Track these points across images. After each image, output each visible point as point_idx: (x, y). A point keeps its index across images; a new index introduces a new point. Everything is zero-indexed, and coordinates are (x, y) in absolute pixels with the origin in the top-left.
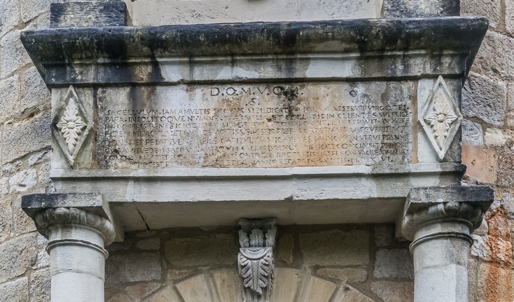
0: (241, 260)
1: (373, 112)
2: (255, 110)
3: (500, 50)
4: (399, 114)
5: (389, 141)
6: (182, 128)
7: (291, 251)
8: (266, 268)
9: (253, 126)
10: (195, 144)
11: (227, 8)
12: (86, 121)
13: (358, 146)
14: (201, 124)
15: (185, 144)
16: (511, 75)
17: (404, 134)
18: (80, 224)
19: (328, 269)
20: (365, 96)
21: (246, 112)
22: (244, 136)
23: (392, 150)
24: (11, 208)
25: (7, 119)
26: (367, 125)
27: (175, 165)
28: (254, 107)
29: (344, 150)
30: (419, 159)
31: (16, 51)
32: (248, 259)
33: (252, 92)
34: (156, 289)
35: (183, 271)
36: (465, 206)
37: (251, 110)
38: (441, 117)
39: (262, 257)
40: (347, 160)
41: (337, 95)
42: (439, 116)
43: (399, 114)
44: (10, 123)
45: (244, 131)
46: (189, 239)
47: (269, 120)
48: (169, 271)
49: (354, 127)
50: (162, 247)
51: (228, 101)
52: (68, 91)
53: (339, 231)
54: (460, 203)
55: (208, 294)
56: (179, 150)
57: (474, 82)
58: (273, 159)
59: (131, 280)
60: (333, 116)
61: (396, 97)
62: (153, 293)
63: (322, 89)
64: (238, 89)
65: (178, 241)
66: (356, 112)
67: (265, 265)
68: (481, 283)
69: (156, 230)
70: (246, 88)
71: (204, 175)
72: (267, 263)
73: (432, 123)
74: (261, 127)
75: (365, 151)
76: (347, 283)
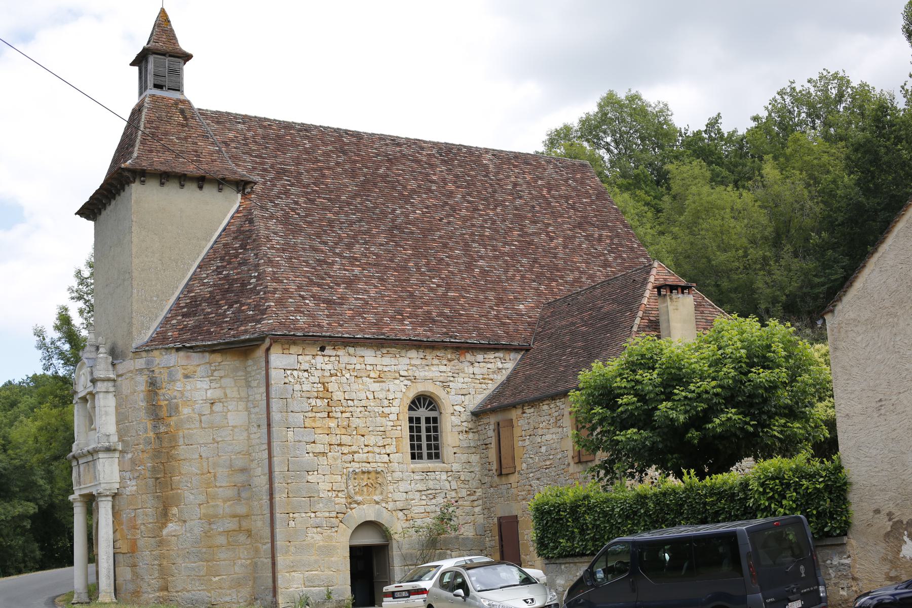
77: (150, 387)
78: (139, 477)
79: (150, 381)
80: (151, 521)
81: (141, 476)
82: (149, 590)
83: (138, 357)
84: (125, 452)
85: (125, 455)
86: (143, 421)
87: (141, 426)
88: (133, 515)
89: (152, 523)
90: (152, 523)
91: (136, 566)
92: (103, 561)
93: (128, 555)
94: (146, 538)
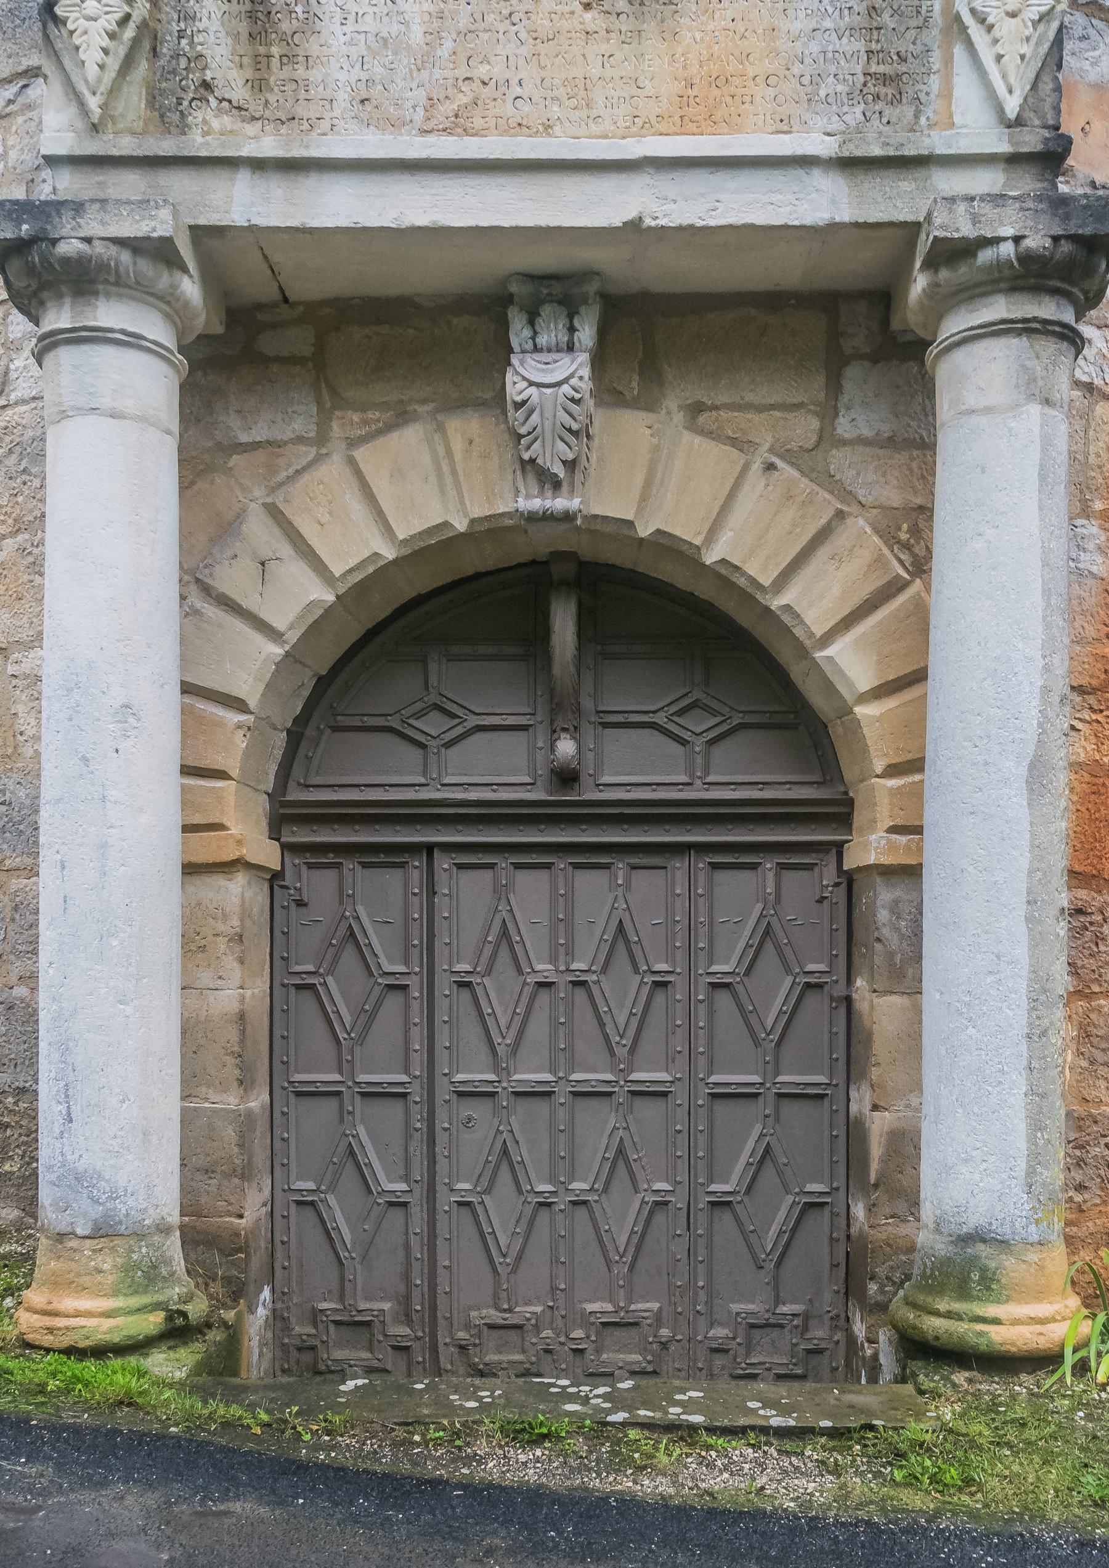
0: (515, 388)
5: (881, 69)
6: (369, 24)
8: (574, 408)
9: (547, 23)
13: (806, 80)
15: (378, 70)
22: (523, 51)
23: (889, 91)
26: (828, 24)
27: (352, 125)
29: (771, 92)
30: (957, 119)
32: (531, 384)
36: (1066, 247)
39: (565, 381)
45: (523, 35)
46: (385, 329)
49: (796, 27)
53: (753, 312)
55: (432, 478)
59: (244, 438)
62: (298, 472)
67: (573, 400)
68: (1098, 455)
72: (577, 396)
73: (990, 20)
74: (566, 25)
75: (823, 94)
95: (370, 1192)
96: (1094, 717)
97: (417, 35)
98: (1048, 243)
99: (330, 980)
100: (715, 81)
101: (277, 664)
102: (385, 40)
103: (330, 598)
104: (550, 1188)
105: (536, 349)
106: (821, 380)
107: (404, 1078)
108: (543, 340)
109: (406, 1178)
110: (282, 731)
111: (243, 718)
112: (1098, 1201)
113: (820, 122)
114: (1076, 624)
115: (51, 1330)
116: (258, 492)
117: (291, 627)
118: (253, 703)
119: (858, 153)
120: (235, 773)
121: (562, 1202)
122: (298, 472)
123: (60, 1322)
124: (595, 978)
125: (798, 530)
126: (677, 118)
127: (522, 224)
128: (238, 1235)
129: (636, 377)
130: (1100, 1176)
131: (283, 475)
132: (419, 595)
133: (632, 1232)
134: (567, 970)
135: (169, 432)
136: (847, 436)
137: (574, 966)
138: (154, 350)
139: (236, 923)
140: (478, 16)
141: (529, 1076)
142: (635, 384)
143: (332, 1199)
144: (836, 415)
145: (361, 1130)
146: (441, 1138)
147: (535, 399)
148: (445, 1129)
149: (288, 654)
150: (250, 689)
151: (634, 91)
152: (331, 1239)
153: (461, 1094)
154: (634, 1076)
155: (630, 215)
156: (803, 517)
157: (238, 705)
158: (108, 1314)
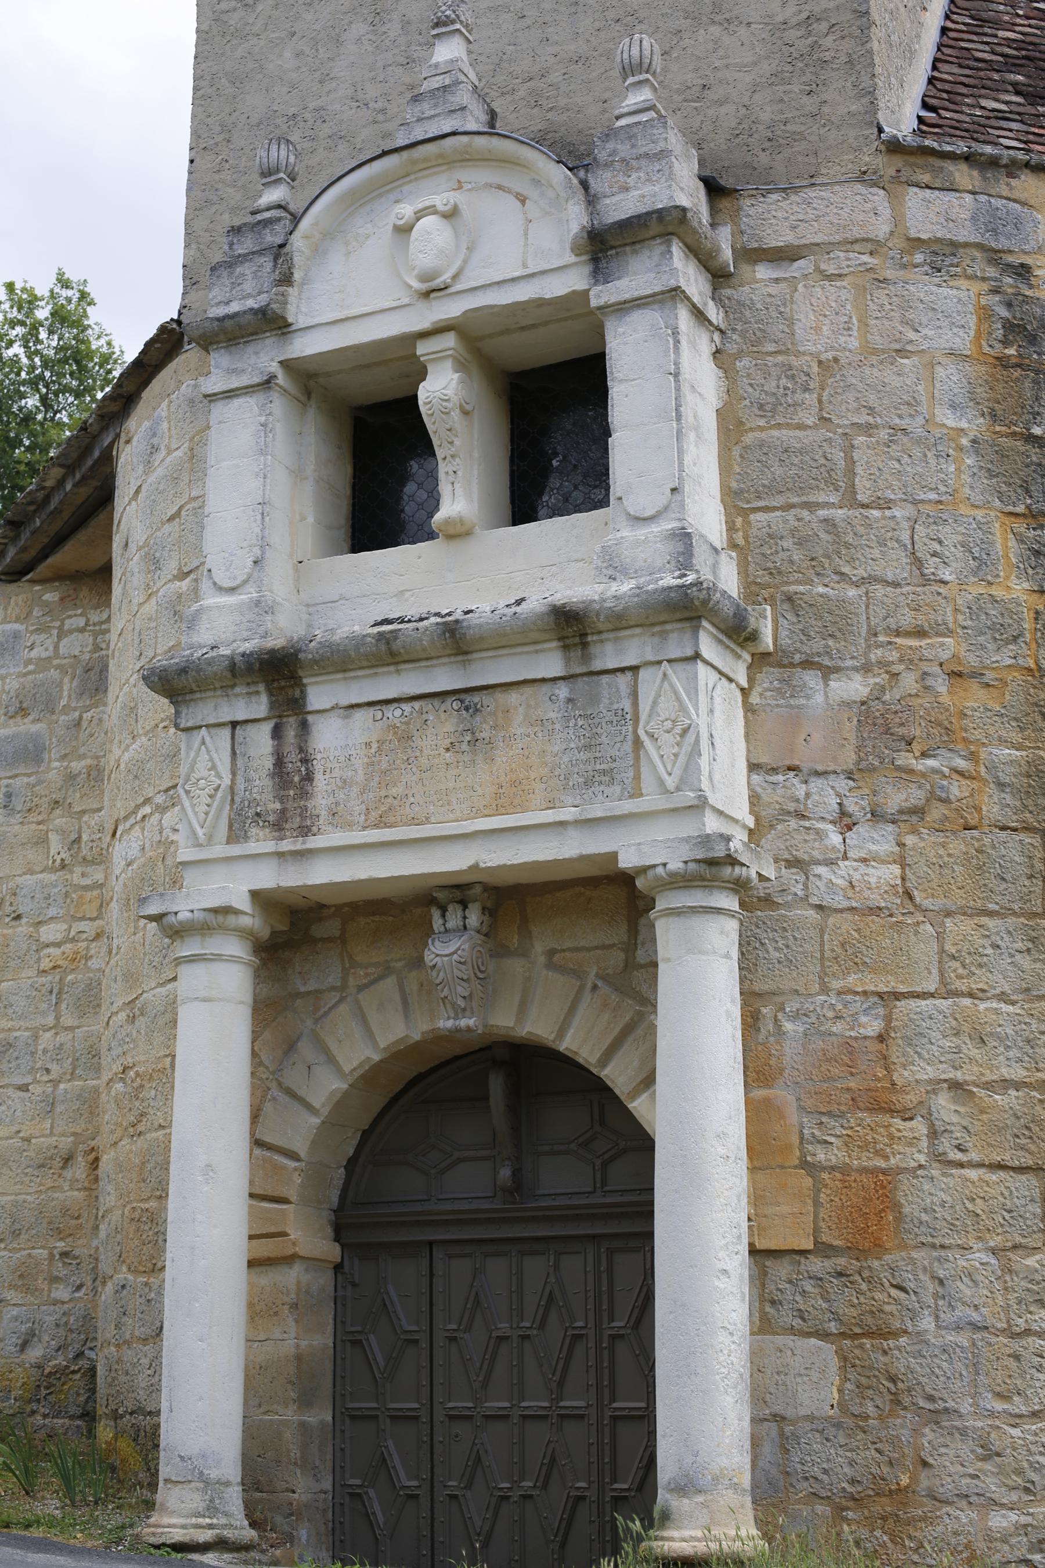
0: (429, 958)
1: (580, 723)
2: (429, 736)
3: (850, 538)
4: (615, 723)
5: (602, 767)
6: (337, 773)
7: (516, 928)
8: (463, 967)
9: (426, 761)
10: (353, 795)
11: (420, 557)
12: (220, 778)
13: (562, 778)
14: (359, 763)
15: (342, 796)
16: (873, 573)
17: (623, 753)
18: (209, 929)
19: (568, 954)
20: (569, 700)
21: (418, 742)
22: (414, 778)
23: (607, 779)
24: (162, 866)
25: (162, 720)
26: (572, 745)
27: (330, 828)
28: (428, 732)
29: (543, 786)
30: (644, 791)
31: (175, 615)
32: (437, 955)
33: (425, 710)
34: (334, 1001)
35: (369, 971)
36: (692, 866)
37: (424, 737)
38: (668, 724)
39: (455, 952)
40: (547, 800)
41: (533, 703)
42: (665, 723)
43: (615, 723)
44: (165, 727)
45: (414, 769)
46: (377, 918)
47: (448, 750)
48: (352, 971)
49: (556, 748)
50: (343, 931)
51: (395, 727)
52: (200, 736)
53: (582, 889)
54: (686, 862)
55: (400, 1008)
56: (333, 806)
57: (801, 602)
58: (452, 808)
59: (303, 989)
60: (528, 736)
61: (610, 699)
62: (330, 1009)
63: (513, 698)
64: (407, 707)
65: (362, 921)
66: (557, 726)
67: (460, 963)
68: (833, 950)
69: (335, 906)
70: (417, 705)
71: (363, 841)
72: (463, 960)
73: (656, 736)
74: (437, 761)
75: (571, 784)
76: (597, 975)
77: (1006, 343)
78: (919, 811)
79: (1004, 313)
80: (1018, 1073)
81: (937, 812)
82: (992, 1486)
83: (926, 178)
84: (807, 664)
85: (811, 679)
86: (964, 510)
87: (950, 535)
88: (872, 1026)
89: (1018, 1085)
90: (1018, 1085)
91: (895, 1334)
92: (722, 1283)
93: (816, 1265)
94: (972, 1174)
95: (395, 1487)
96: (844, 1132)
97: (360, 777)
98: (681, 865)
99: (372, 1337)
100: (514, 784)
101: (317, 1129)
102: (345, 781)
103: (345, 1086)
104: (508, 1485)
105: (446, 931)
106: (625, 927)
107: (416, 1405)
108: (450, 925)
109: (417, 1477)
110: (339, 1168)
111: (297, 1164)
112: (871, 1493)
113: (570, 800)
114: (822, 1069)
115: (154, 1534)
116: (309, 1022)
117: (323, 1105)
118: (303, 1154)
119: (589, 817)
120: (293, 1199)
121: (515, 1495)
122: (330, 1009)
123: (159, 1530)
124: (535, 1332)
125: (612, 1026)
126: (494, 806)
127: (415, 873)
128: (291, 1504)
129: (516, 936)
130: (871, 1473)
131: (323, 1010)
132: (421, 1074)
133: (561, 1519)
134: (518, 1327)
135: (241, 1003)
136: (642, 962)
137: (522, 1325)
138: (233, 959)
139: (293, 1296)
140: (391, 762)
141: (497, 1404)
142: (515, 941)
143: (372, 1493)
144: (636, 948)
145: (390, 1443)
146: (438, 1449)
147: (440, 964)
148: (441, 1442)
149: (323, 1122)
150: (301, 1147)
151: (472, 793)
152: (370, 1521)
153: (451, 1418)
154: (562, 1404)
155: (471, 862)
156: (615, 1017)
157: (293, 1156)
158: (184, 1527)
